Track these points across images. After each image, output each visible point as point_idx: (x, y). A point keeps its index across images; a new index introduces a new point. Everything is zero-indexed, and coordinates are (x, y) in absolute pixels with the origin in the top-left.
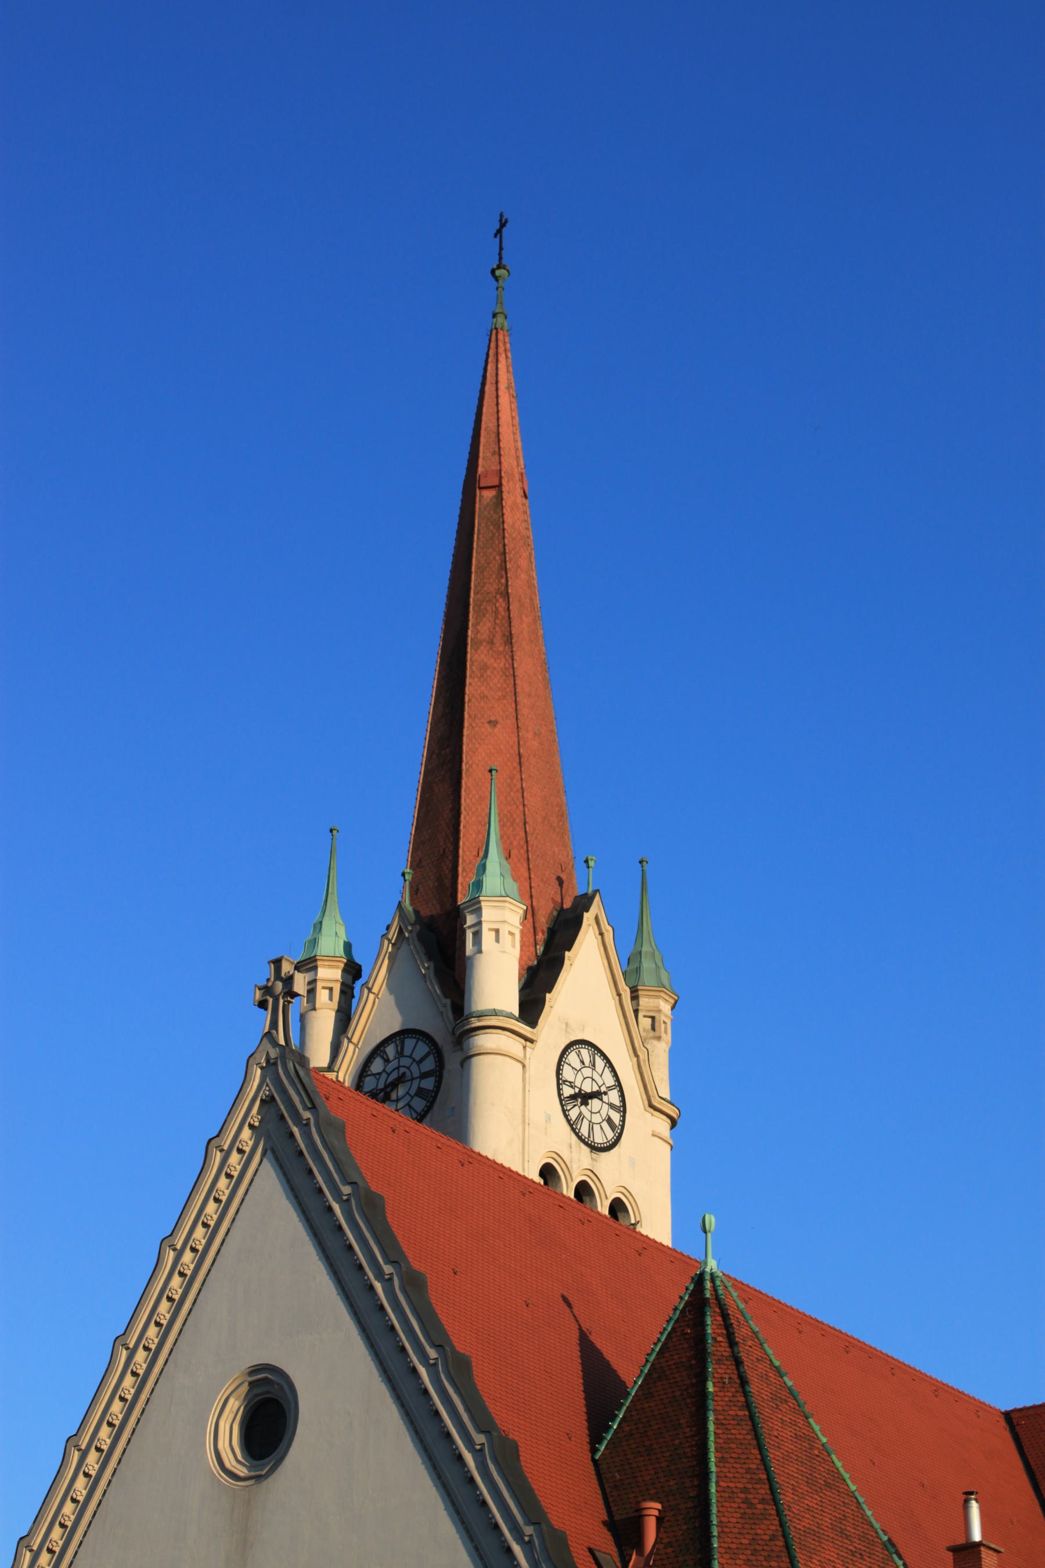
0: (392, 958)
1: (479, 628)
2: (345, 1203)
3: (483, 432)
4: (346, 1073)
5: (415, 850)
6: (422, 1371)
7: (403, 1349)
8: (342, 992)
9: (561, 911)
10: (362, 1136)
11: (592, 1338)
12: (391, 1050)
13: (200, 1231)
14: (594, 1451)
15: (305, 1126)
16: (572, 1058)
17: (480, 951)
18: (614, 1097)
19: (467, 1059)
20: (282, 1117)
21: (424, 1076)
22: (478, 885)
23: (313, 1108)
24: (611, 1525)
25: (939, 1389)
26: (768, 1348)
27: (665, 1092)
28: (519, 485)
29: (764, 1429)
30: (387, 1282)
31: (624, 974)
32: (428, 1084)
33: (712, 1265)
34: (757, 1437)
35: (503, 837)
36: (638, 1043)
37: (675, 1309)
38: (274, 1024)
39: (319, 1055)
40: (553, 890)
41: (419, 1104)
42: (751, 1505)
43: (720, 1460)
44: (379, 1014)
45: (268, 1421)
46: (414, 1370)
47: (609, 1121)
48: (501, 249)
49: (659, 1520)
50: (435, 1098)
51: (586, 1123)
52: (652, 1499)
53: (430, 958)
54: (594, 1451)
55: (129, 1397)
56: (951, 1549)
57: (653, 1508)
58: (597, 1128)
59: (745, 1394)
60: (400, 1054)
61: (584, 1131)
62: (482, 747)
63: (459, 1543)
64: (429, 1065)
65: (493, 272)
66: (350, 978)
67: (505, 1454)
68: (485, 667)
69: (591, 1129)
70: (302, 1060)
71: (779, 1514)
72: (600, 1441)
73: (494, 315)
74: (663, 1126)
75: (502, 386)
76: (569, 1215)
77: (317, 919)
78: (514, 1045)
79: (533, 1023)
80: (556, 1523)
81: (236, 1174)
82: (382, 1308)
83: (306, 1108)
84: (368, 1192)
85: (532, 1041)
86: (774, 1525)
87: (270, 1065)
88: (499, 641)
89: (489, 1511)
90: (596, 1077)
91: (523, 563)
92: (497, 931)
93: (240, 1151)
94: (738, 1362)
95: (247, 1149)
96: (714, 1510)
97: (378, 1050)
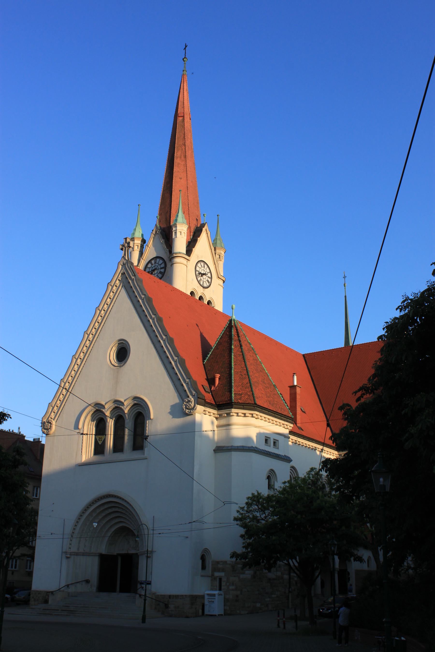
0: (154, 238)
1: (177, 154)
2: (143, 300)
3: (180, 102)
4: (142, 267)
5: (160, 211)
6: (162, 341)
7: (157, 336)
8: (141, 247)
9: (197, 227)
10: (146, 282)
11: (203, 334)
12: (153, 262)
13: (106, 306)
14: (203, 362)
15: (133, 280)
16: (199, 265)
17: (176, 237)
18: (209, 275)
19: (172, 265)
20: (127, 278)
21: (161, 268)
22: (176, 220)
23: (135, 276)
24: (207, 379)
25: (287, 348)
26: (247, 338)
27: (222, 274)
28: (189, 116)
29: (246, 358)
30: (153, 319)
31: (213, 244)
32: (162, 270)
33: (234, 317)
34: (244, 359)
35: (183, 208)
38: (125, 254)
39: (135, 264)
40: (195, 222)
41: (160, 275)
42: (242, 375)
43: (235, 365)
44: (150, 252)
45: (123, 353)
46: (159, 341)
47: (208, 281)
49: (219, 379)
50: (164, 274)
51: (202, 281)
52: (217, 374)
53: (163, 238)
54: (203, 362)
55: (88, 346)
56: (289, 387)
57: (218, 376)
58: (205, 282)
59: (241, 349)
60: (155, 263)
61: (202, 283)
62: (178, 184)
63: (170, 383)
64: (163, 265)
65: (183, 59)
66: (143, 243)
67: (182, 362)
68: (179, 164)
69: (203, 283)
70: (132, 264)
71: (249, 378)
72: (205, 359)
73: (183, 71)
74: (221, 282)
75: (185, 90)
76: (197, 304)
77: (135, 228)
78: (184, 261)
80: (194, 379)
81: (115, 292)
82: (152, 326)
83: (133, 276)
84: (148, 297)
85: (189, 260)
86: (248, 380)
87: (124, 264)
88: (183, 157)
89: (178, 375)
90: (205, 270)
91: (189, 137)
92: (181, 232)
93: (116, 286)
94: (240, 341)
95: (118, 286)
96: (233, 376)
97: (150, 262)
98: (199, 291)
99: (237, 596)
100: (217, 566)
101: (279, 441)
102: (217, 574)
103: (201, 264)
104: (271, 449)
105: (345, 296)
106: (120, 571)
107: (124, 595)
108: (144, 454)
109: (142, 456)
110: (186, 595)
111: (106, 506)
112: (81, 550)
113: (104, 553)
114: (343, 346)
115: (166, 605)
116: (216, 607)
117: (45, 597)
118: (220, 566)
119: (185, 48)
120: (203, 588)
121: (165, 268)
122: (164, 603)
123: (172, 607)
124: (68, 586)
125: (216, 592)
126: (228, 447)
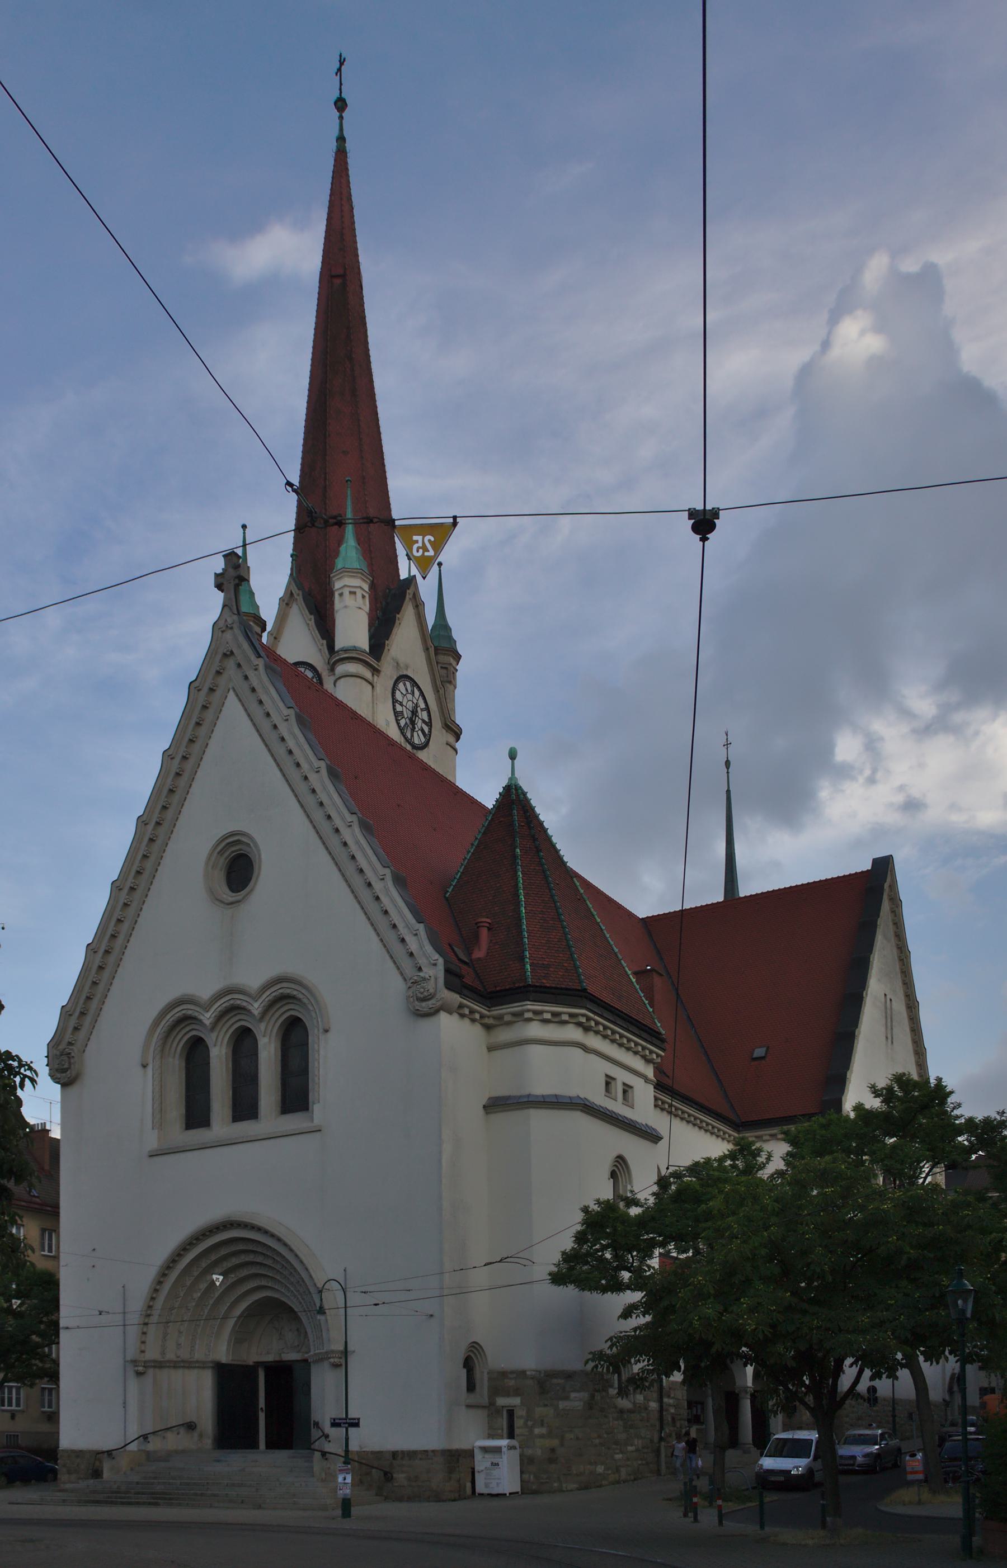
16: (401, 686)
36: (439, 683)
37: (469, 852)
45: (238, 868)
48: (341, 84)
79: (378, 659)
99: (553, 1450)
100: (503, 1381)
101: (635, 1089)
102: (501, 1401)
103: (405, 685)
104: (617, 1107)
105: (728, 792)
106: (266, 1406)
107: (281, 1456)
108: (312, 1121)
110: (433, 1451)
111: (223, 1251)
112: (170, 1356)
113: (224, 1360)
115: (386, 1473)
116: (501, 1474)
117: (94, 1463)
119: (339, 70)
120: (471, 1434)
122: (381, 1472)
123: (400, 1477)
124: (145, 1437)
125: (504, 1443)
126: (520, 1097)
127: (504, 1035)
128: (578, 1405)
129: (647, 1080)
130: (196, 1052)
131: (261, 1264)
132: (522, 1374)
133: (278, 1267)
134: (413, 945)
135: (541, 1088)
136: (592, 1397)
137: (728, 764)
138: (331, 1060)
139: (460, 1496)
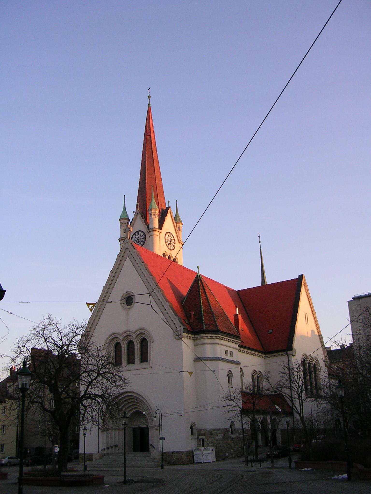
12: (137, 234)
16: (167, 235)
32: (143, 240)
45: (129, 300)
60: (138, 235)
64: (143, 236)
79: (161, 230)
98: (169, 252)
100: (200, 432)
102: (200, 437)
104: (229, 358)
109: (148, 366)
114: (260, 285)
117: (89, 457)
118: (203, 432)
121: (145, 238)
122: (167, 459)
127: (198, 342)
128: (221, 437)
129: (236, 349)
130: (118, 346)
131: (133, 402)
132: (205, 430)
133: (140, 403)
134: (175, 321)
135: (209, 355)
136: (224, 435)
137: (260, 241)
138: (154, 350)
139: (190, 463)
